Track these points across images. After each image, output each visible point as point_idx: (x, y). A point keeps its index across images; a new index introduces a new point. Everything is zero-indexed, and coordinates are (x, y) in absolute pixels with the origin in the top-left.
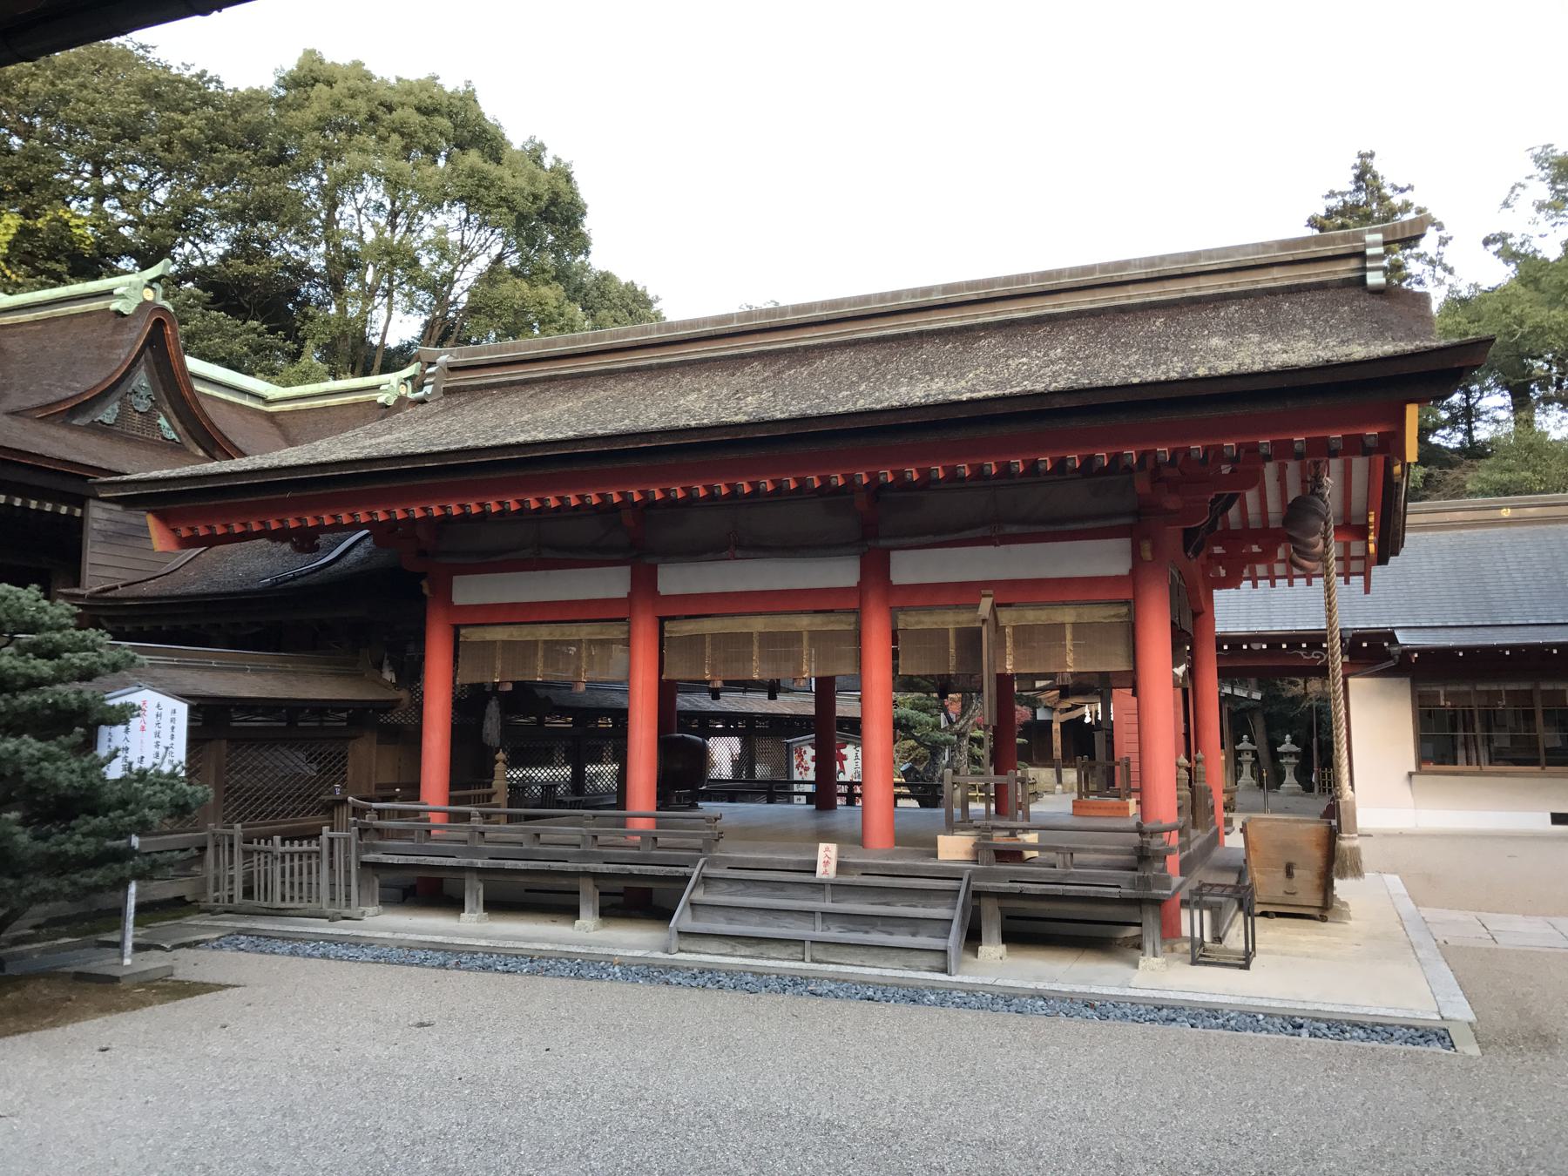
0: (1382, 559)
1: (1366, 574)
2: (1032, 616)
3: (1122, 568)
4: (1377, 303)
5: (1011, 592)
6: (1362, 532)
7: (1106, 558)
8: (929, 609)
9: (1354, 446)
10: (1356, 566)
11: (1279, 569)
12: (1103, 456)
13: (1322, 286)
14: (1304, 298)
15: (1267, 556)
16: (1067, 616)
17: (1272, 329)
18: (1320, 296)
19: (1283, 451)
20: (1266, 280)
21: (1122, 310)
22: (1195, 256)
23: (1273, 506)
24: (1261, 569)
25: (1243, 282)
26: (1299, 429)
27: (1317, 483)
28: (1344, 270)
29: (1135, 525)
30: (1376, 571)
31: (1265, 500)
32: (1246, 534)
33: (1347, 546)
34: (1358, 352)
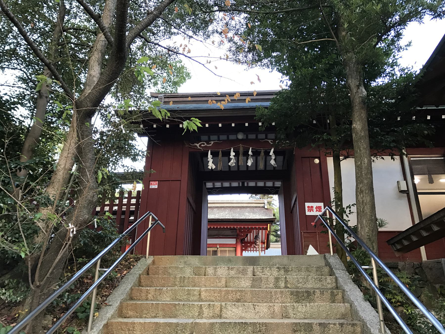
0: (267, 249)
1: (264, 251)
2: (222, 249)
3: (235, 243)
4: (266, 210)
5: (222, 245)
6: (264, 243)
7: (232, 241)
8: (418, 165)
9: (263, 229)
10: (263, 249)
11: (252, 249)
12: (215, 227)
13: (259, 207)
14: (257, 208)
15: (250, 246)
16: (227, 249)
17: (254, 213)
18: (259, 208)
19: (256, 229)
20: (252, 205)
21: (233, 207)
22: (243, 201)
23: (252, 238)
24: (249, 249)
25: (249, 205)
26: (257, 226)
27: (258, 233)
28: (262, 205)
29: (236, 237)
30: (266, 251)
31: (250, 237)
32: (248, 242)
33: (262, 246)
34: (264, 218)
